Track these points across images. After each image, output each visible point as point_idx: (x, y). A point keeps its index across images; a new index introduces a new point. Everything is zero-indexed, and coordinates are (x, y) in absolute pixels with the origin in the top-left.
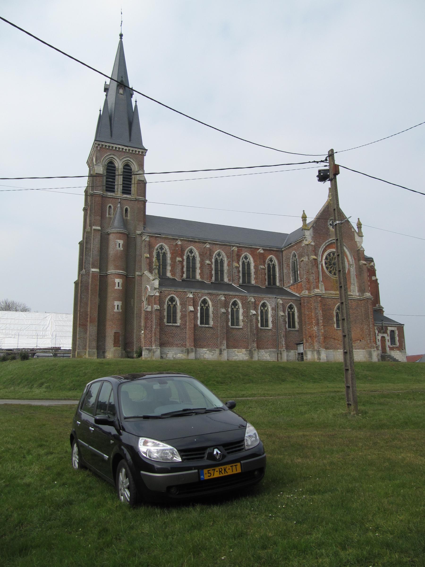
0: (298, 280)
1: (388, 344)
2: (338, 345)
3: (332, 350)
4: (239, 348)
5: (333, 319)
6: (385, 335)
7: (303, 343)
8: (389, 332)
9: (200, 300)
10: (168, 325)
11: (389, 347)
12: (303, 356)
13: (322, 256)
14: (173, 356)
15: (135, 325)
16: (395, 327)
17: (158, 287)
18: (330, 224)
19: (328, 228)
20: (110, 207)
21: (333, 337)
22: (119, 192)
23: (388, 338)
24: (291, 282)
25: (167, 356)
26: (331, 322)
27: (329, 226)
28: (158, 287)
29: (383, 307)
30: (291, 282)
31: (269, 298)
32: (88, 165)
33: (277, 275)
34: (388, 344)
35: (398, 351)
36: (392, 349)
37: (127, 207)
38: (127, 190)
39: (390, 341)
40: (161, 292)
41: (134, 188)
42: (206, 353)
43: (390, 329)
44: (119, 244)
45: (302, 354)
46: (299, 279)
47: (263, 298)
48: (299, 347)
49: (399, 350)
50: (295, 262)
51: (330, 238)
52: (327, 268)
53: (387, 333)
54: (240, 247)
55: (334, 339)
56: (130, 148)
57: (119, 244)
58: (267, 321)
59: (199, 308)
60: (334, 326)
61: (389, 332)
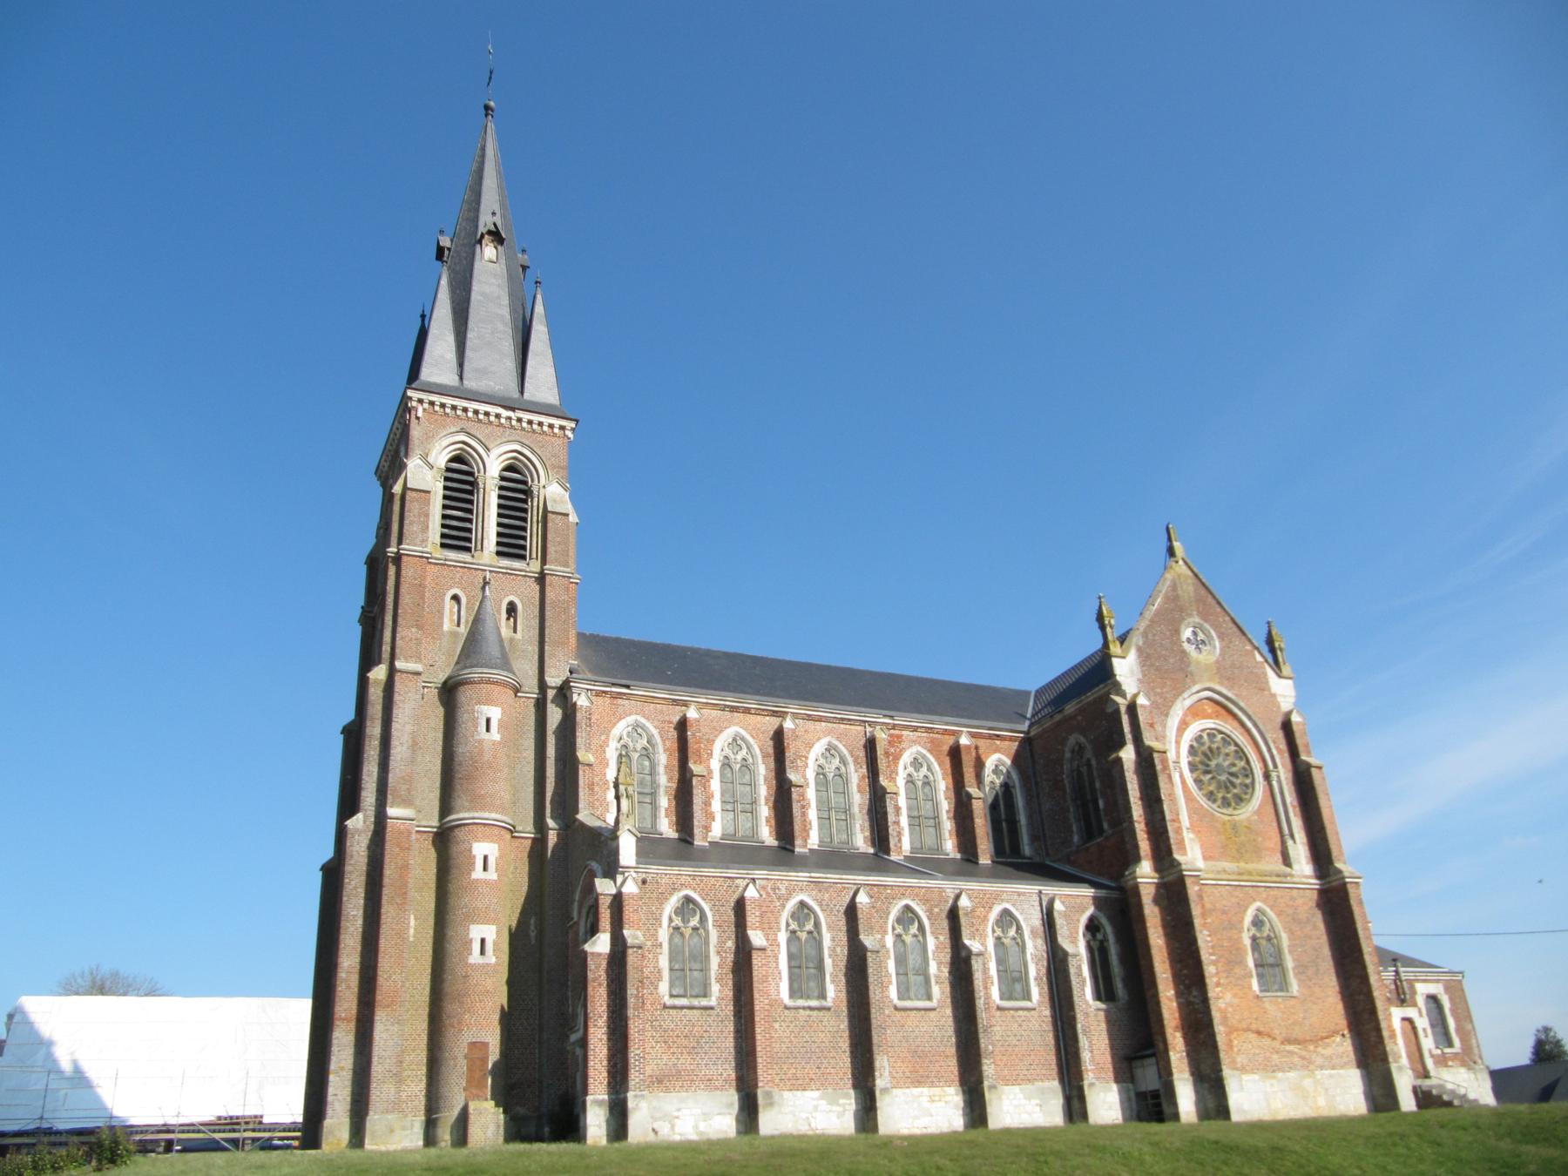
0: (1101, 831)
1: (1428, 1043)
2: (1275, 1056)
3: (1256, 1077)
4: (932, 1085)
5: (1242, 962)
6: (1411, 1012)
7: (1153, 1055)
8: (1420, 1000)
9: (783, 906)
10: (674, 1007)
11: (1432, 1056)
12: (1159, 1105)
13: (1178, 743)
14: (696, 1127)
15: (812, 814)
16: (1437, 981)
17: (633, 864)
18: (1189, 640)
19: (1184, 652)
20: (456, 598)
21: (1254, 1027)
22: (492, 468)
23: (1422, 1023)
24: (1076, 838)
25: (673, 1127)
26: (1238, 971)
27: (1186, 646)
28: (633, 864)
29: (258, 1113)
30: (1076, 838)
31: (1019, 894)
32: (379, 478)
33: (1023, 819)
34: (1428, 1043)
35: (1463, 1070)
36: (1442, 1061)
37: (512, 598)
38: (511, 546)
39: (1429, 1031)
40: (644, 882)
41: (533, 541)
42: (816, 1108)
43: (1423, 989)
44: (488, 720)
45: (1155, 1095)
46: (1106, 826)
47: (997, 897)
48: (1139, 1072)
49: (1463, 1064)
50: (1084, 770)
51: (1194, 683)
52: (1198, 781)
53: (1414, 1005)
54: (894, 727)
55: (1259, 1033)
56: (520, 414)
57: (488, 720)
58: (1023, 978)
59: (783, 937)
60: (1250, 987)
61: (1420, 1000)
